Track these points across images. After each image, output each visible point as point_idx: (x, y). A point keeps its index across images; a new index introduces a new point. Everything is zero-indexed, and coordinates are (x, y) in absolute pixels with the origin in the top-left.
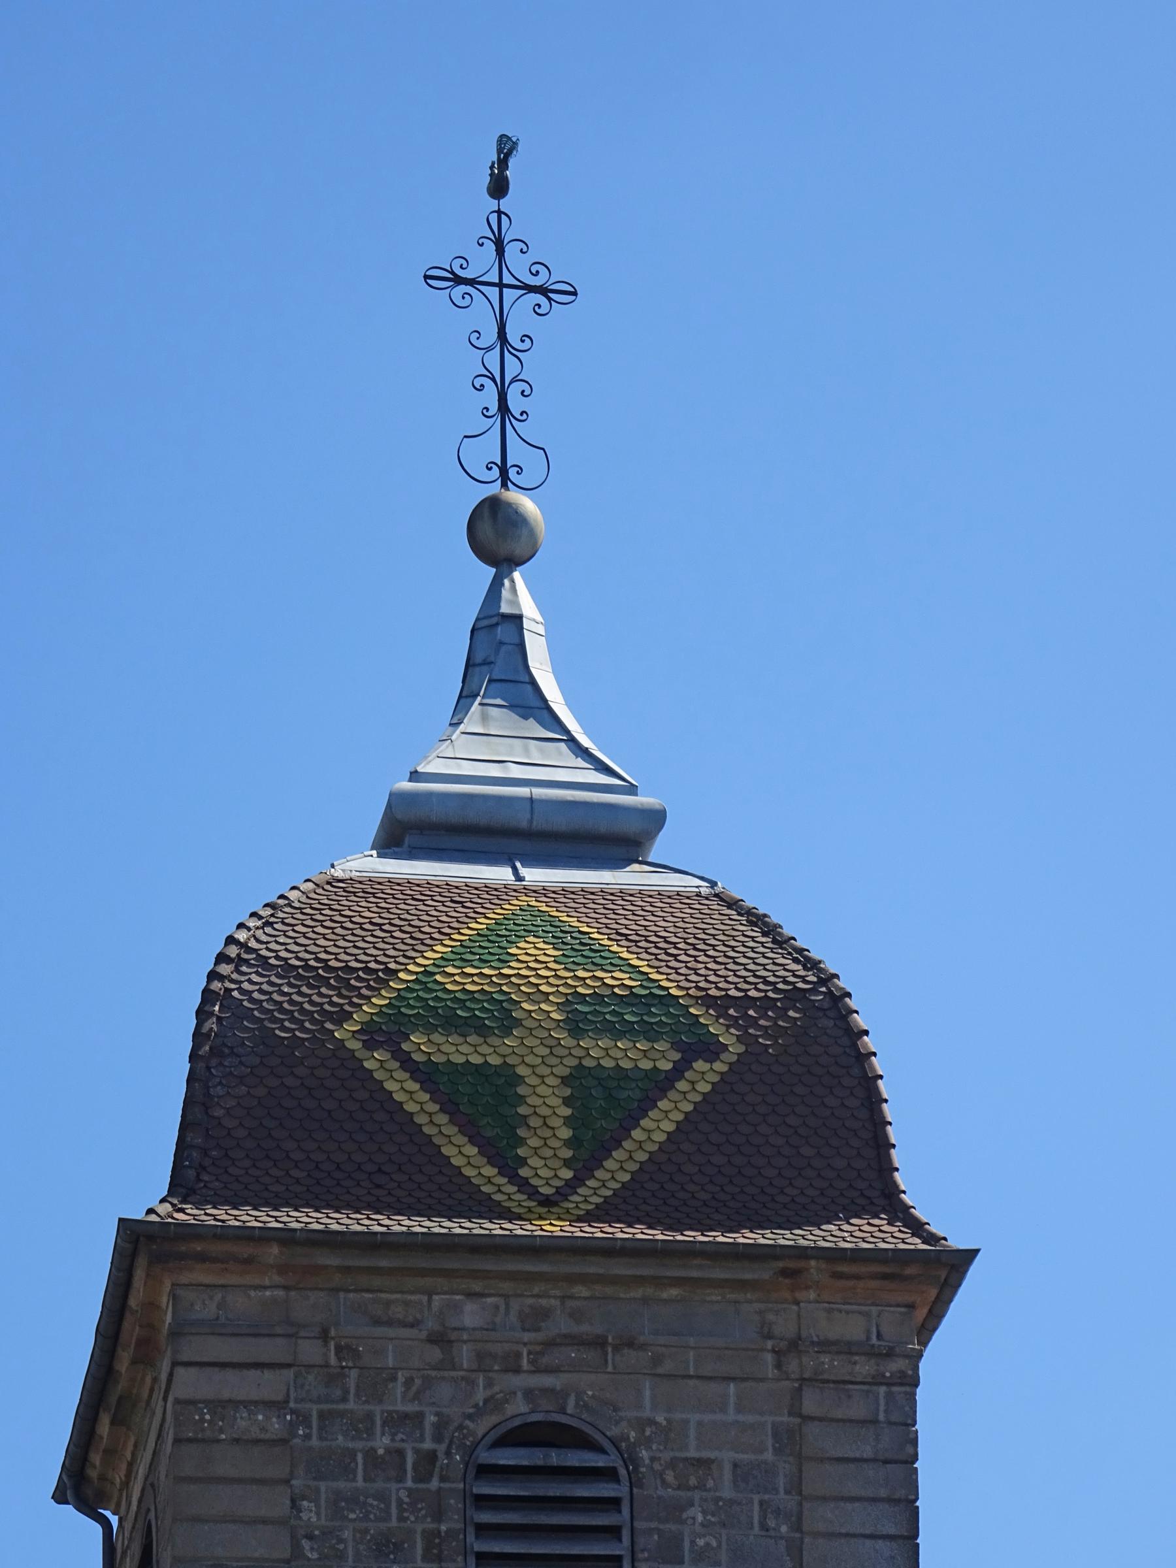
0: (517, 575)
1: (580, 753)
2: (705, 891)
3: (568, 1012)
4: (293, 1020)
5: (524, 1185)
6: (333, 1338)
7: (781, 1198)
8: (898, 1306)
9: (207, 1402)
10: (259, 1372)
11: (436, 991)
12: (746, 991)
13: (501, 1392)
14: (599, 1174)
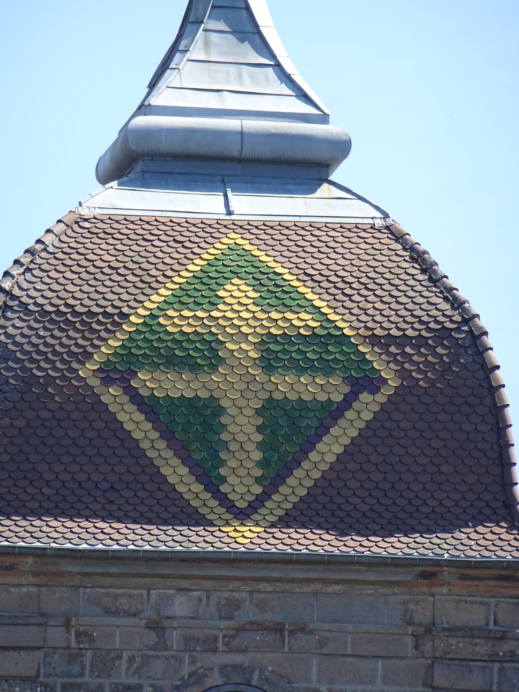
1: (284, 78)
2: (379, 223)
3: (263, 351)
4: (47, 360)
5: (223, 499)
6: (74, 626)
7: (426, 509)
8: (511, 597)
10: (16, 653)
11: (159, 333)
12: (404, 330)
13: (202, 667)
14: (283, 489)
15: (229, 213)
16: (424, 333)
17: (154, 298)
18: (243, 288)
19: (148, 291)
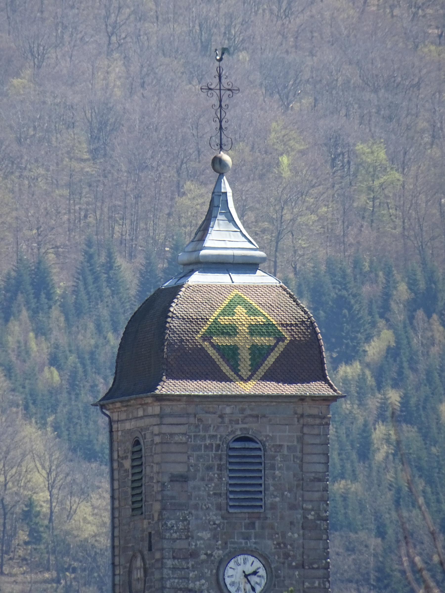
0: (225, 178)
7: (300, 378)
9: (169, 434)
14: (257, 373)
15: (233, 282)
16: (297, 323)
17: (216, 313)
18: (242, 309)
19: (213, 310)
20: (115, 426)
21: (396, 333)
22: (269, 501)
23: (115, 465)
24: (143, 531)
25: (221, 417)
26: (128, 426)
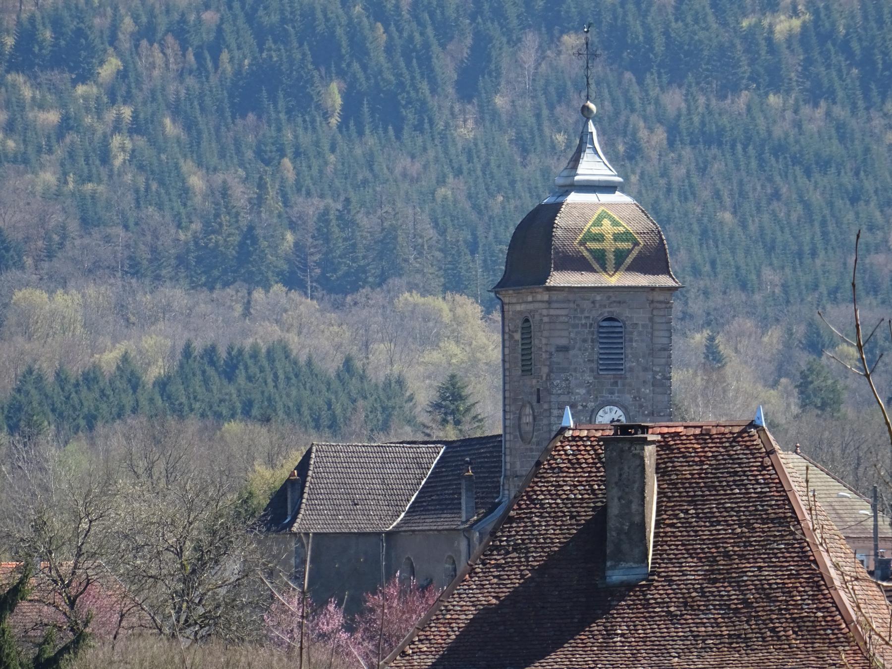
20: (506, 307)
21: (123, 61)
22: (628, 365)
23: (507, 337)
24: (532, 387)
25: (593, 302)
26: (518, 308)
